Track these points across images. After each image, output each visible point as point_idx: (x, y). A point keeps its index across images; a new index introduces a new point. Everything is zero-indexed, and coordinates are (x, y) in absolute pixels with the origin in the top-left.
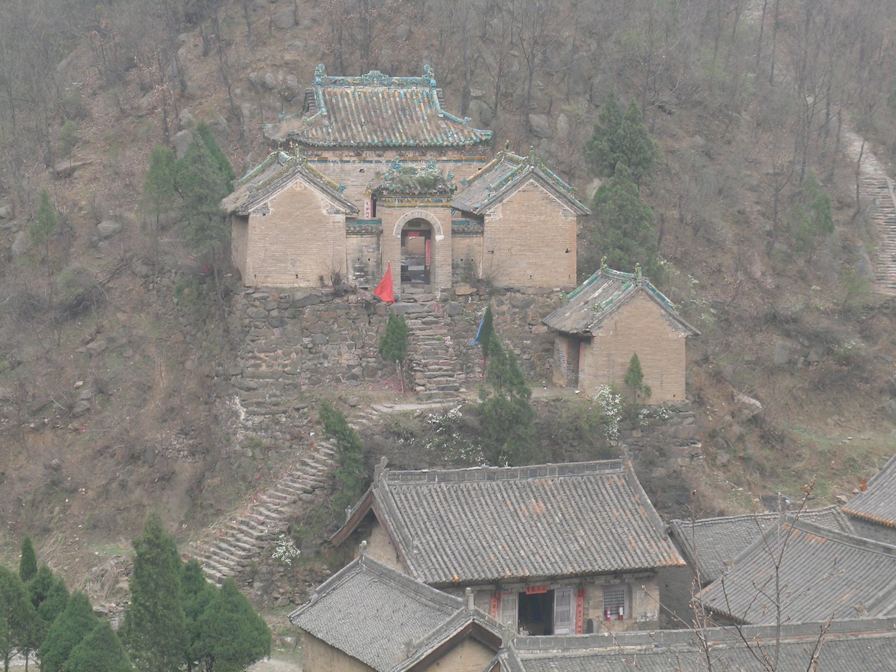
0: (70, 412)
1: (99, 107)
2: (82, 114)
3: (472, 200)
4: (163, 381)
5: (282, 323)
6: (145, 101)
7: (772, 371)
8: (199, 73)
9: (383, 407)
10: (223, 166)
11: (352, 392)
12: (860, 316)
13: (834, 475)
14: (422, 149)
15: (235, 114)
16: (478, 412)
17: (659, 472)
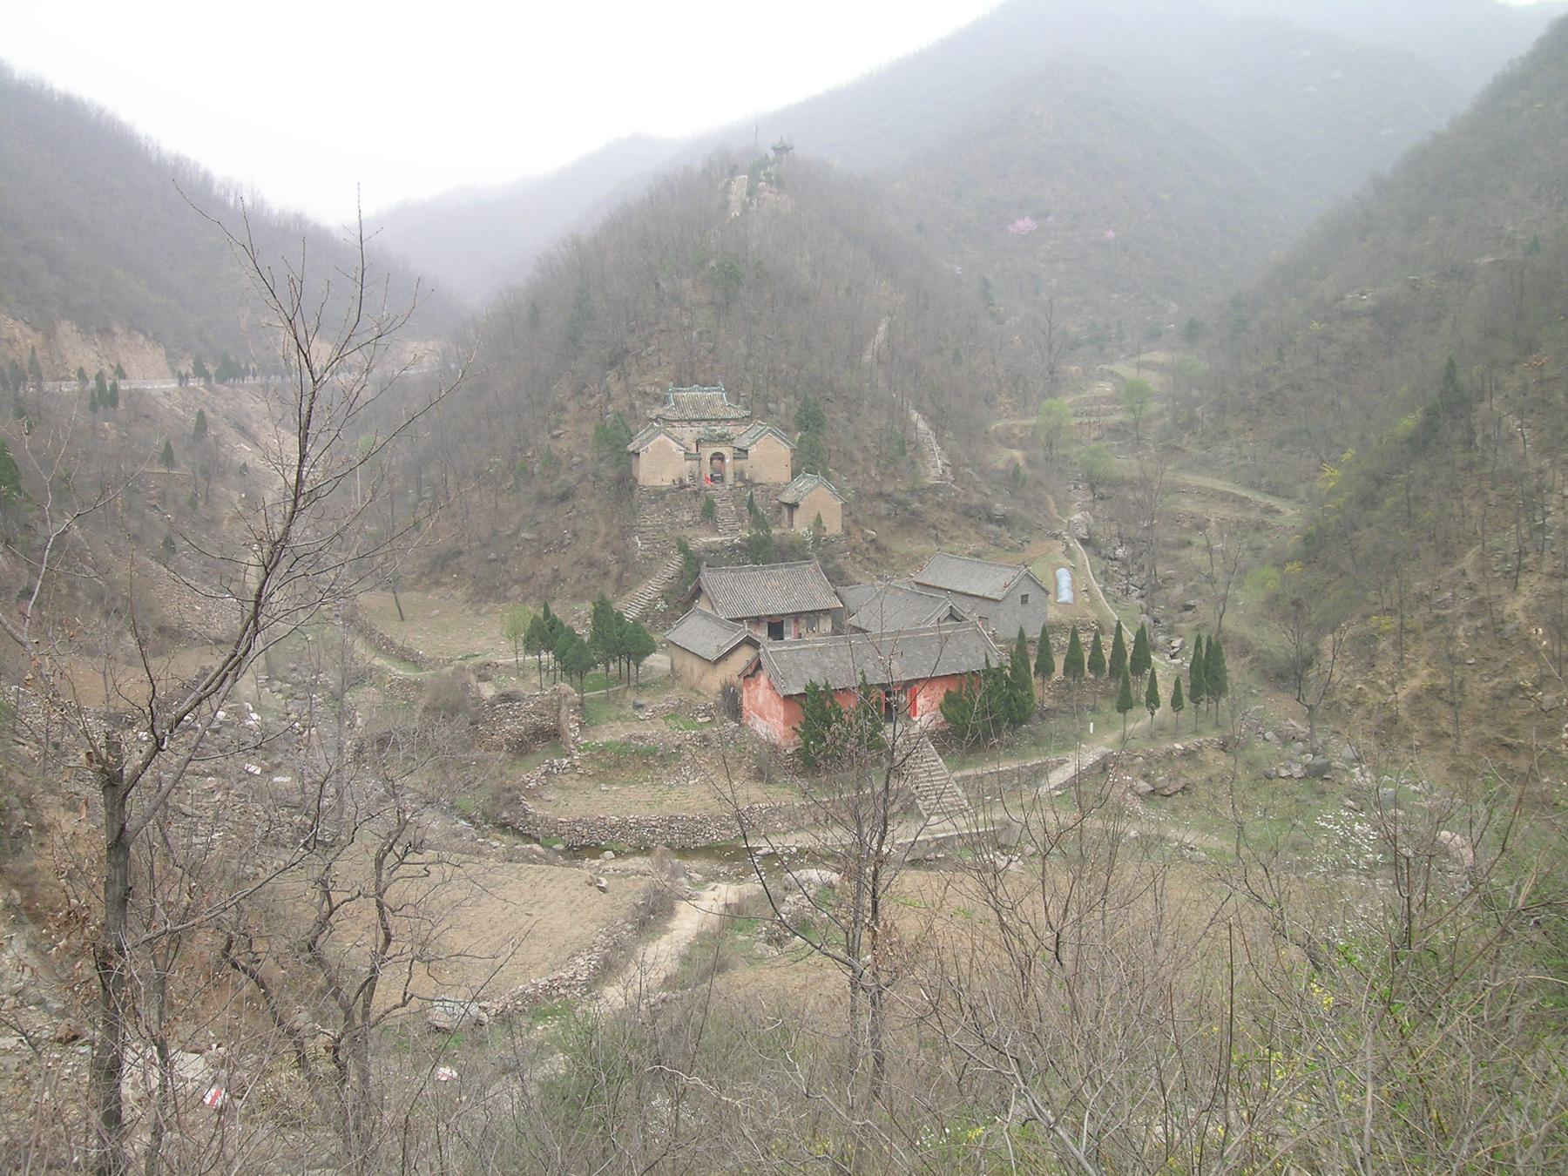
0: (561, 545)
1: (571, 406)
2: (564, 409)
3: (742, 443)
4: (603, 529)
5: (656, 502)
6: (591, 402)
7: (880, 518)
8: (616, 389)
9: (703, 539)
10: (628, 430)
11: (689, 533)
12: (920, 493)
13: (909, 565)
14: (719, 420)
15: (632, 407)
16: (748, 540)
17: (831, 566)
